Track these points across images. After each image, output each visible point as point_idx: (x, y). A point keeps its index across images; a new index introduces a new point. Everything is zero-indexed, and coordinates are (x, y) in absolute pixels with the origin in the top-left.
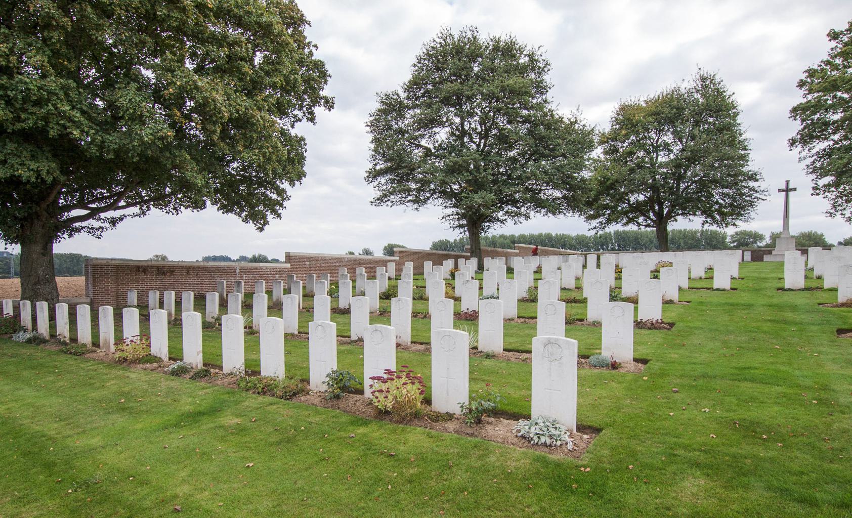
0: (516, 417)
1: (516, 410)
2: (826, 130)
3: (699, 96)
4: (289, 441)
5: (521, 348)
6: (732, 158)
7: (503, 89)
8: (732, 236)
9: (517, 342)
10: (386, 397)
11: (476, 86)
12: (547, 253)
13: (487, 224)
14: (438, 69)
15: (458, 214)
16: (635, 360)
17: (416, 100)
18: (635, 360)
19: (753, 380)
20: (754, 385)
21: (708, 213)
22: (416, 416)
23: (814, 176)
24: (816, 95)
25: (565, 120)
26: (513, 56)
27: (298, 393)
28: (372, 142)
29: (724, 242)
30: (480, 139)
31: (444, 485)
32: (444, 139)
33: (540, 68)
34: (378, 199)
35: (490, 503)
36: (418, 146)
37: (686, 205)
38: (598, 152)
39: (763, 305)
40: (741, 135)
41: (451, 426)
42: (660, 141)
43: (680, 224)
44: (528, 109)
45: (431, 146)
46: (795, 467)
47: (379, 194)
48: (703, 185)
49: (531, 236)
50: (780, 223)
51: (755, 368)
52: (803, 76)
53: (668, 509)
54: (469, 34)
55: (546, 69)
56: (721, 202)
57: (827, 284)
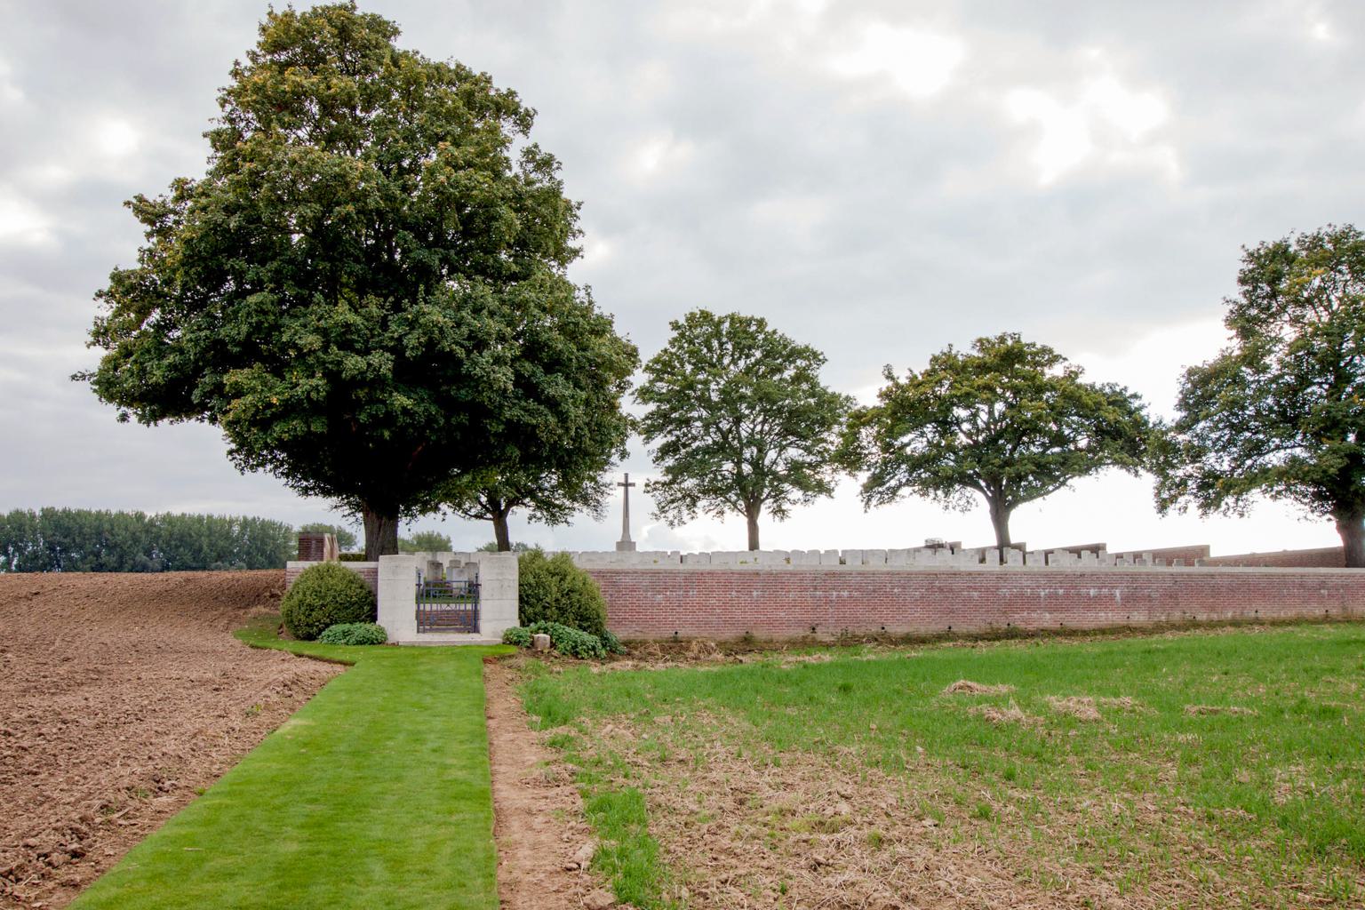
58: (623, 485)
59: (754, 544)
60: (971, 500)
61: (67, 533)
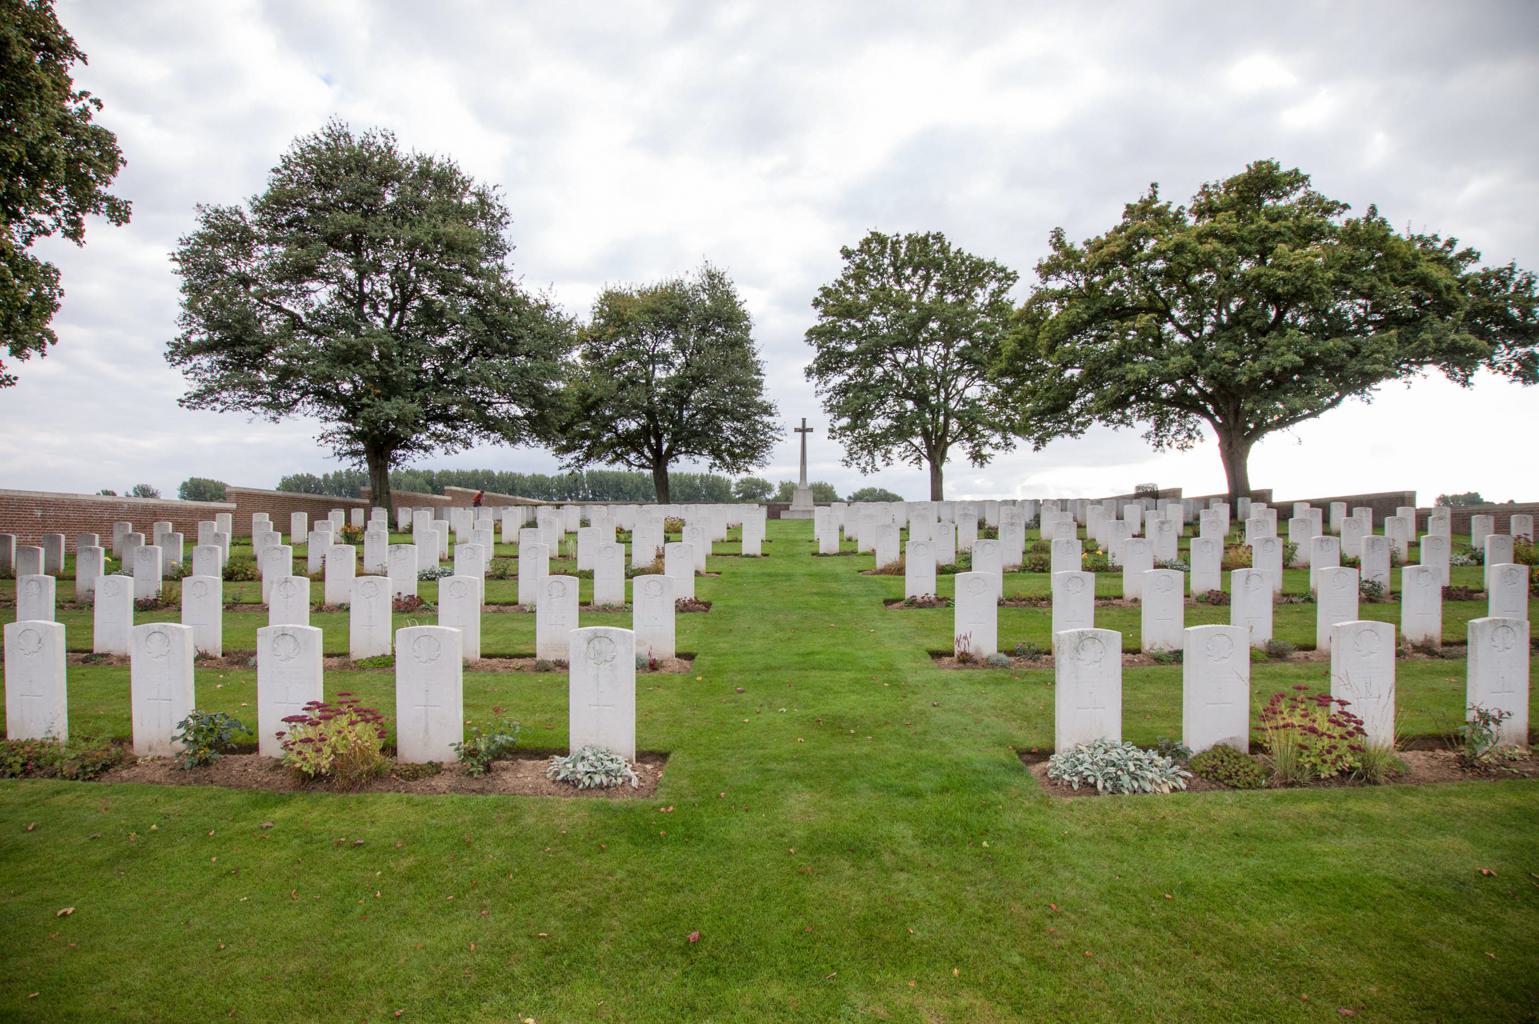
0: (542, 754)
1: (539, 744)
2: (840, 361)
3: (706, 297)
4: (133, 855)
5: (507, 651)
6: (743, 383)
7: (437, 240)
8: (737, 485)
9: (497, 643)
10: (319, 750)
11: (389, 227)
12: (507, 503)
13: (400, 452)
14: (320, 185)
15: (349, 432)
16: (678, 655)
17: (276, 228)
18: (678, 655)
19: (820, 667)
20: (823, 673)
21: (716, 453)
22: (377, 775)
23: (830, 416)
24: (831, 319)
25: (531, 301)
26: (452, 191)
27: (113, 765)
28: (183, 290)
29: (728, 492)
30: (393, 312)
31: (471, 873)
32: (324, 302)
33: (493, 216)
34: (196, 396)
35: (554, 883)
36: (278, 309)
37: (693, 439)
38: (575, 356)
39: (804, 575)
40: (754, 355)
41: (441, 782)
42: (657, 349)
43: (688, 466)
44: (474, 276)
45: (299, 311)
46: (892, 761)
47: (195, 387)
48: (712, 414)
49: (460, 474)
50: (797, 469)
51: (819, 653)
52: (818, 294)
53: (782, 835)
54: (380, 141)
55: (503, 221)
56: (732, 439)
57: (862, 548)
58: (800, 430)
59: (937, 494)
60: (1194, 434)
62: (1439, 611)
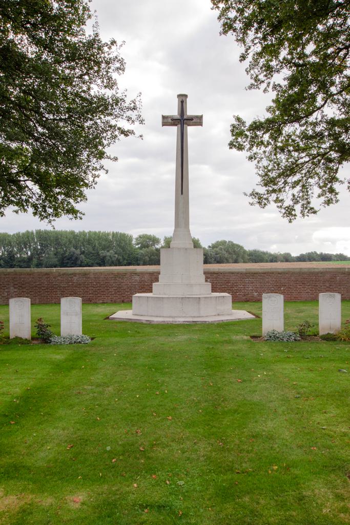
8: (137, 239)
61: (46, 239)
62: (340, 307)
